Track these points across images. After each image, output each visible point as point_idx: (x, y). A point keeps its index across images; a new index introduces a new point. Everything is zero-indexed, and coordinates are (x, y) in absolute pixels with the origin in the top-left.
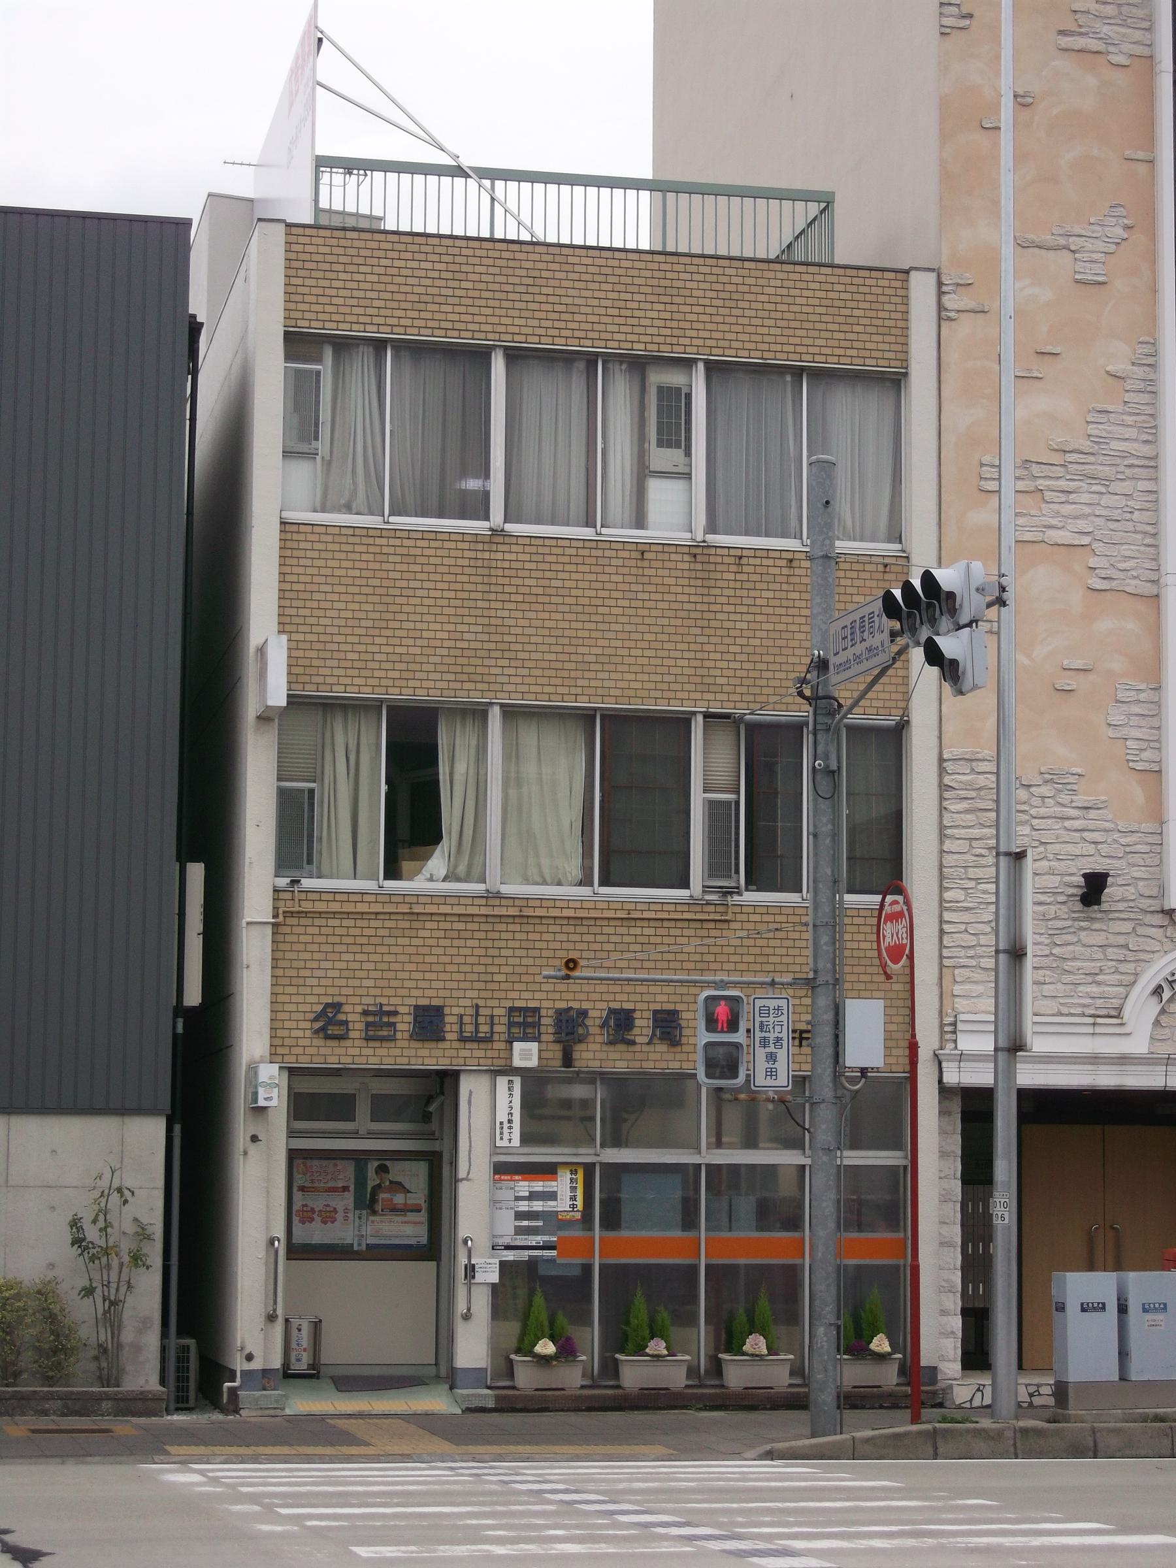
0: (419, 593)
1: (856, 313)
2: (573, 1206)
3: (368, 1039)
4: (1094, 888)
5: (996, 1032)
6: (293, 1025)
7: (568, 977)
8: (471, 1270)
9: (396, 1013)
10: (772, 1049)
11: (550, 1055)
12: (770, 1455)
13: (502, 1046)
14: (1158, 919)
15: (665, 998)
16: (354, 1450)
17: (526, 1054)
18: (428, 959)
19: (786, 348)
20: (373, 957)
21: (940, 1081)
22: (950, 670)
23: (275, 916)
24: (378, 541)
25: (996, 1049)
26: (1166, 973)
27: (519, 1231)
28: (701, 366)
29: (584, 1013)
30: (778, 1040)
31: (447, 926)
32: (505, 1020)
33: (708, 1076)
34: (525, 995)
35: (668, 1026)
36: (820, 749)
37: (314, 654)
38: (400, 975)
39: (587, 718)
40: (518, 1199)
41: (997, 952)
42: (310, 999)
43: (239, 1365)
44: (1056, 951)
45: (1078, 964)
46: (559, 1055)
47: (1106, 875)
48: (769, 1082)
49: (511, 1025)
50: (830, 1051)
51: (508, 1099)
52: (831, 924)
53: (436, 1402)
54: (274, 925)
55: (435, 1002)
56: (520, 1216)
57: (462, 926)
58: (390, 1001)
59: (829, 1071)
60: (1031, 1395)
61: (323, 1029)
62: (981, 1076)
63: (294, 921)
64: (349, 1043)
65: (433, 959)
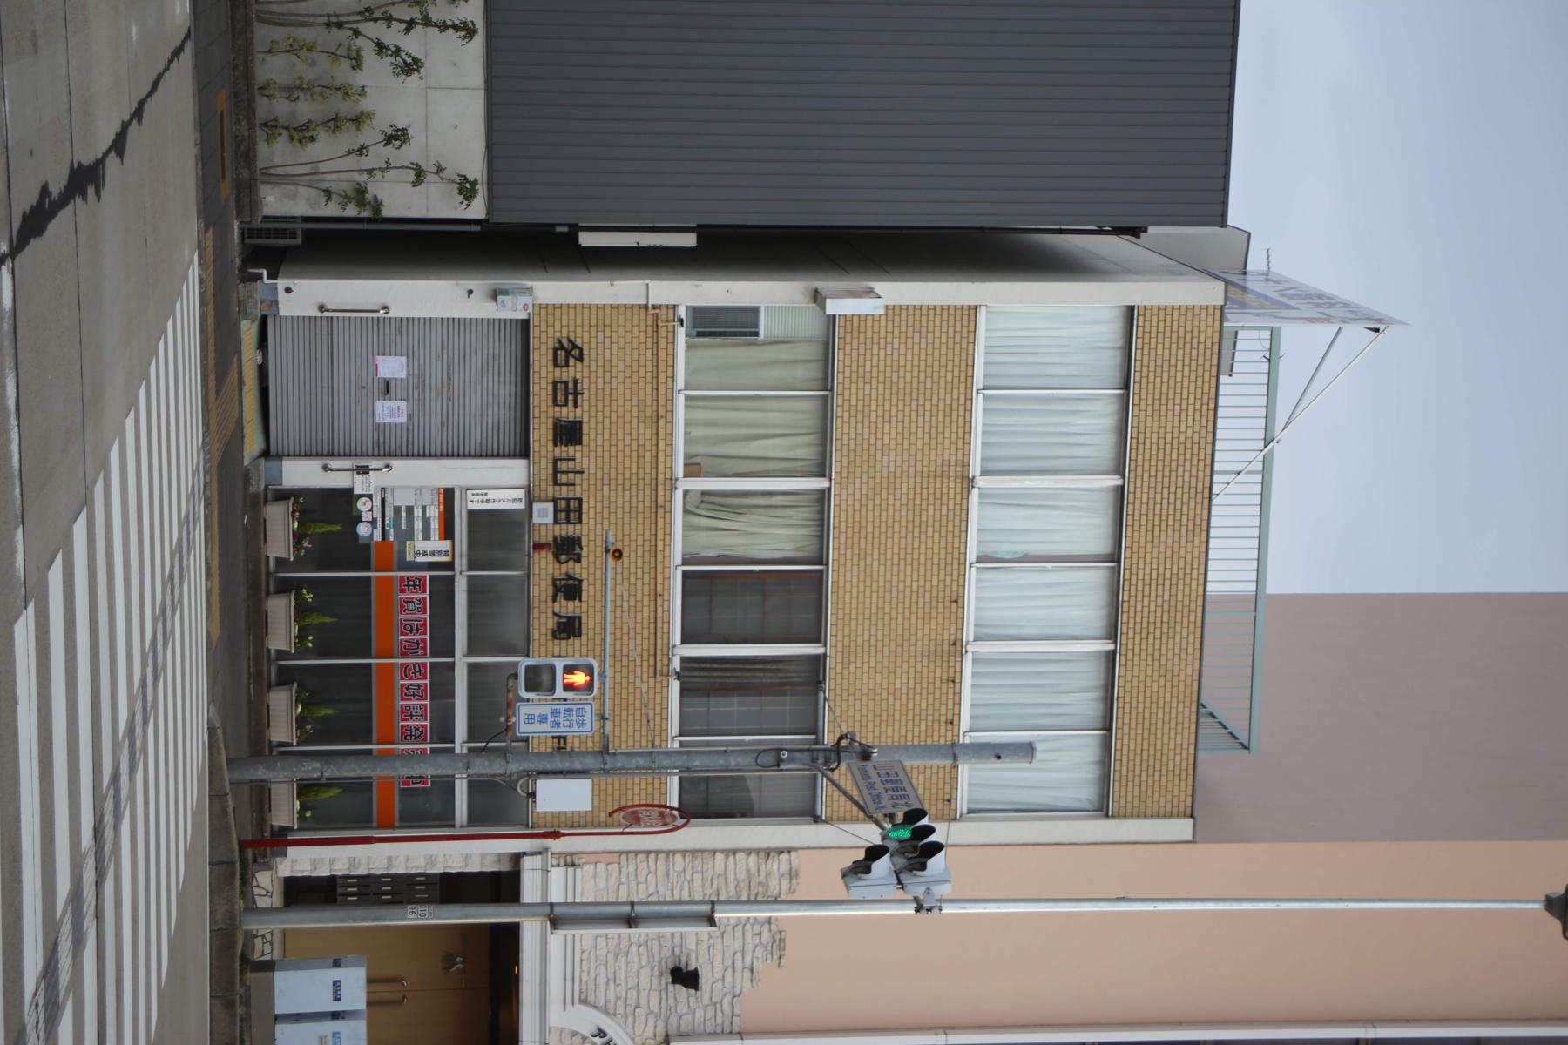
0: (921, 420)
1: (1157, 774)
2: (418, 554)
3: (555, 383)
4: (686, 977)
5: (566, 904)
6: (565, 322)
7: (607, 551)
8: (364, 470)
9: (576, 406)
10: (550, 719)
11: (543, 532)
12: (212, 731)
13: (550, 494)
14: (661, 1031)
15: (591, 626)
16: (212, 385)
17: (543, 514)
18: (620, 432)
19: (1127, 717)
20: (621, 387)
21: (525, 854)
22: (861, 868)
23: (654, 307)
24: (962, 386)
25: (552, 905)
26: (616, 1039)
27: (397, 510)
28: (1112, 647)
29: (578, 560)
30: (558, 724)
31: (649, 402)
32: (571, 495)
33: (528, 668)
34: (592, 512)
35: (568, 628)
36: (797, 755)
37: (869, 334)
38: (607, 410)
39: (821, 559)
40: (424, 509)
41: (632, 904)
42: (586, 336)
43: (281, 283)
44: (634, 949)
45: (623, 966)
46: (543, 540)
47: (696, 988)
48: (523, 718)
49: (568, 500)
50: (549, 767)
51: (508, 500)
52: (652, 761)
53: (253, 443)
54: (646, 307)
55: (585, 438)
56: (410, 510)
57: (648, 459)
58: (583, 401)
59: (532, 767)
60: (263, 936)
61: (562, 347)
62: (530, 891)
63: (650, 322)
64: (551, 368)
65: (620, 436)
